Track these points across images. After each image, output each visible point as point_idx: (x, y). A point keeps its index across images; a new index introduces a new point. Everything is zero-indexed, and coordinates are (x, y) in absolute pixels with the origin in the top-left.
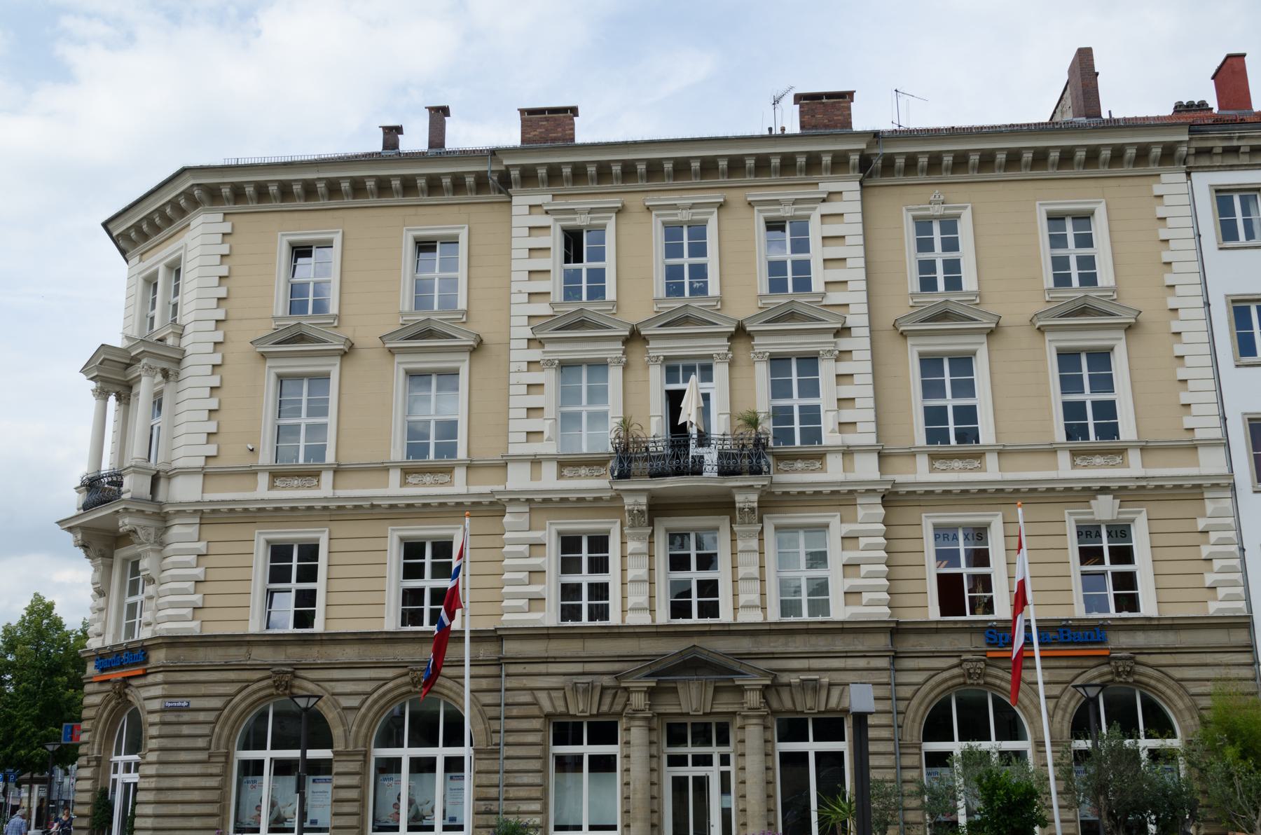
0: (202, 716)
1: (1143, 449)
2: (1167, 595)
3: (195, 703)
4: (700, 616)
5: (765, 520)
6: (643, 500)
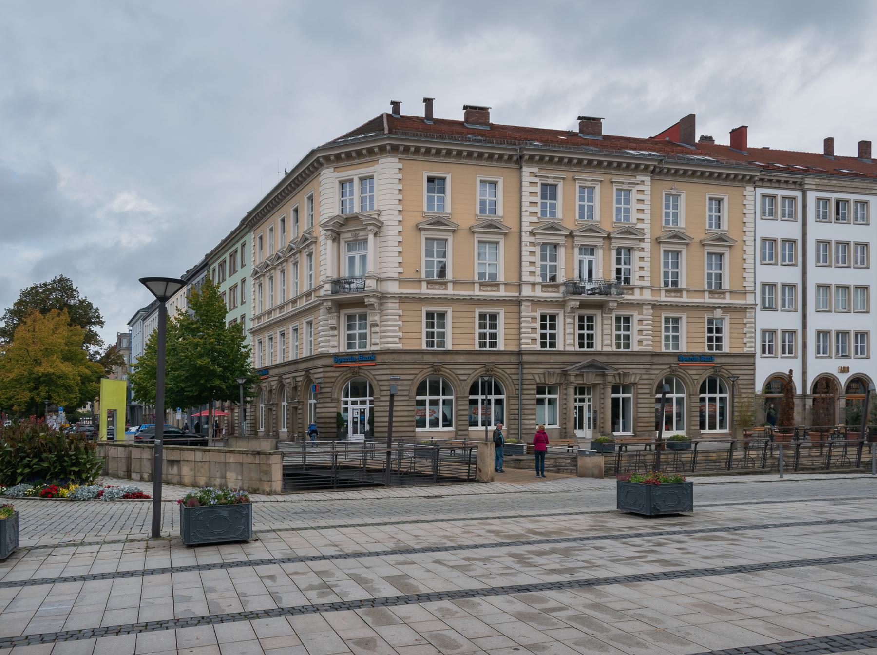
0: (406, 383)
1: (505, 284)
2: (456, 341)
3: (403, 377)
4: (489, 347)
6: (578, 303)
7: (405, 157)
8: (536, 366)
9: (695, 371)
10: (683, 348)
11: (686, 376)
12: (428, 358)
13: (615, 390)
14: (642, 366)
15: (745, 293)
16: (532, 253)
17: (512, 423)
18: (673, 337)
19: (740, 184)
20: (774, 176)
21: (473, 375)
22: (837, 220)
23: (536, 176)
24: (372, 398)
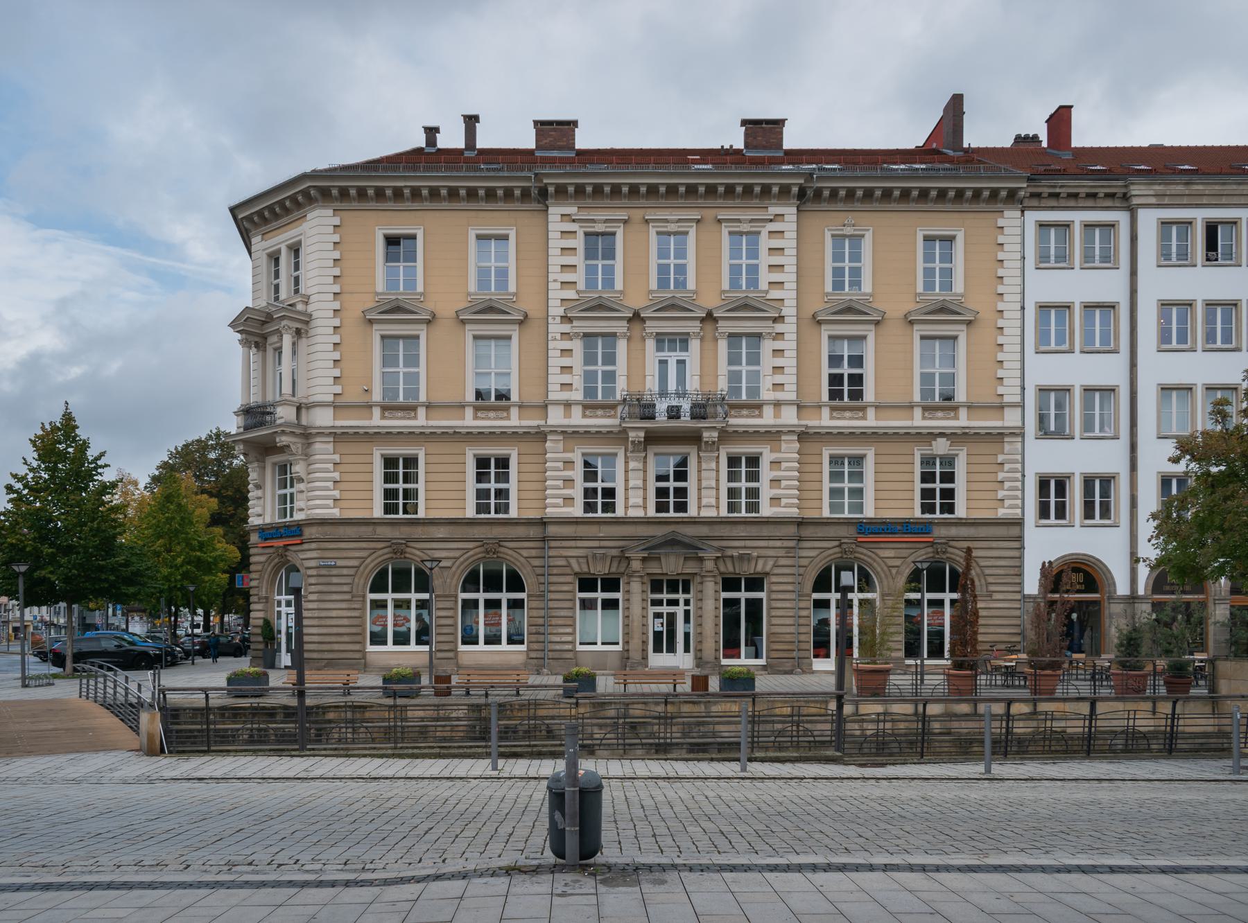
0: (345, 571)
1: (876, 407)
2: (881, 504)
3: (340, 563)
5: (721, 450)
6: (642, 434)
7: (344, 205)
8: (572, 543)
9: (893, 551)
10: (869, 512)
11: (875, 561)
12: (478, 532)
13: (730, 584)
14: (778, 544)
15: (1002, 407)
16: (566, 352)
17: (534, 640)
18: (851, 490)
19: (991, 207)
20: (1061, 187)
21: (818, 559)
22: (1208, 260)
23: (574, 221)
24: (425, 596)
